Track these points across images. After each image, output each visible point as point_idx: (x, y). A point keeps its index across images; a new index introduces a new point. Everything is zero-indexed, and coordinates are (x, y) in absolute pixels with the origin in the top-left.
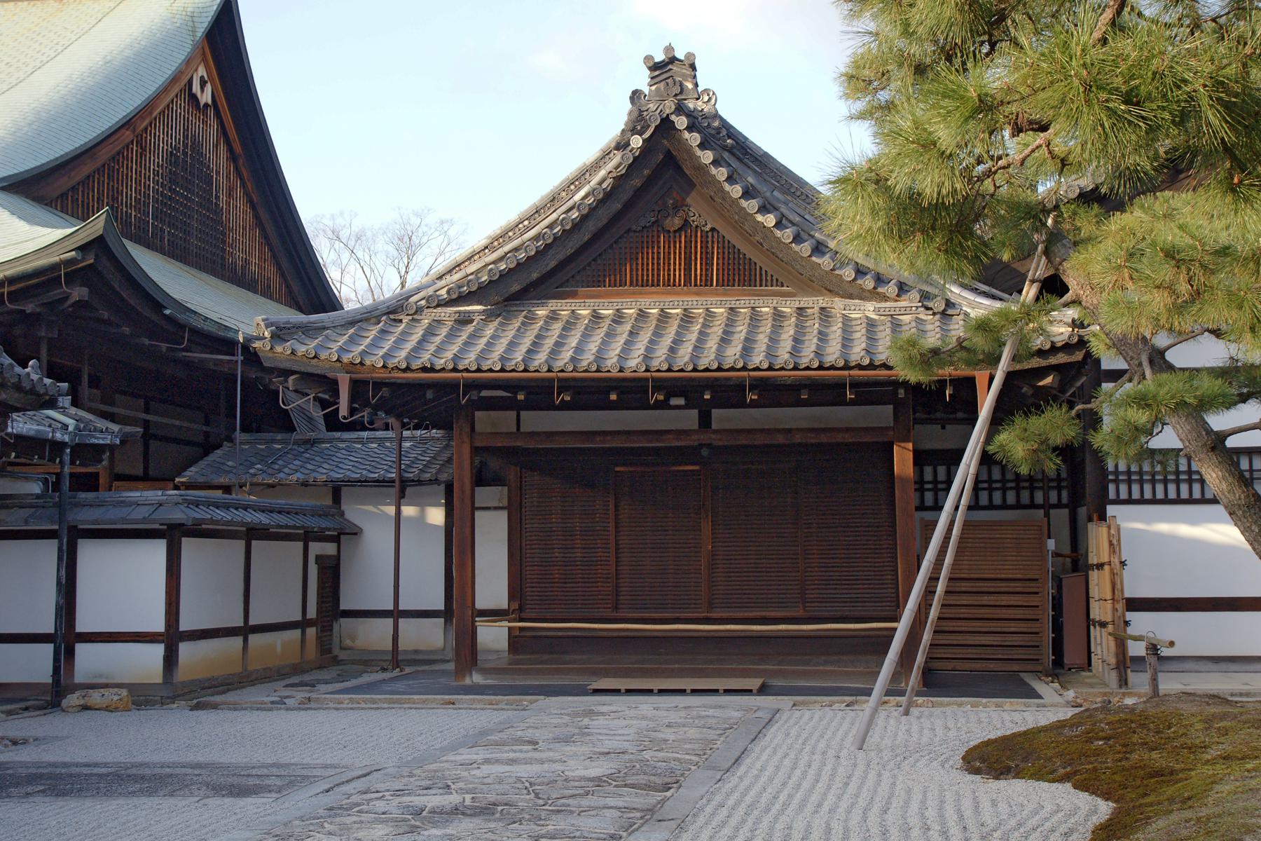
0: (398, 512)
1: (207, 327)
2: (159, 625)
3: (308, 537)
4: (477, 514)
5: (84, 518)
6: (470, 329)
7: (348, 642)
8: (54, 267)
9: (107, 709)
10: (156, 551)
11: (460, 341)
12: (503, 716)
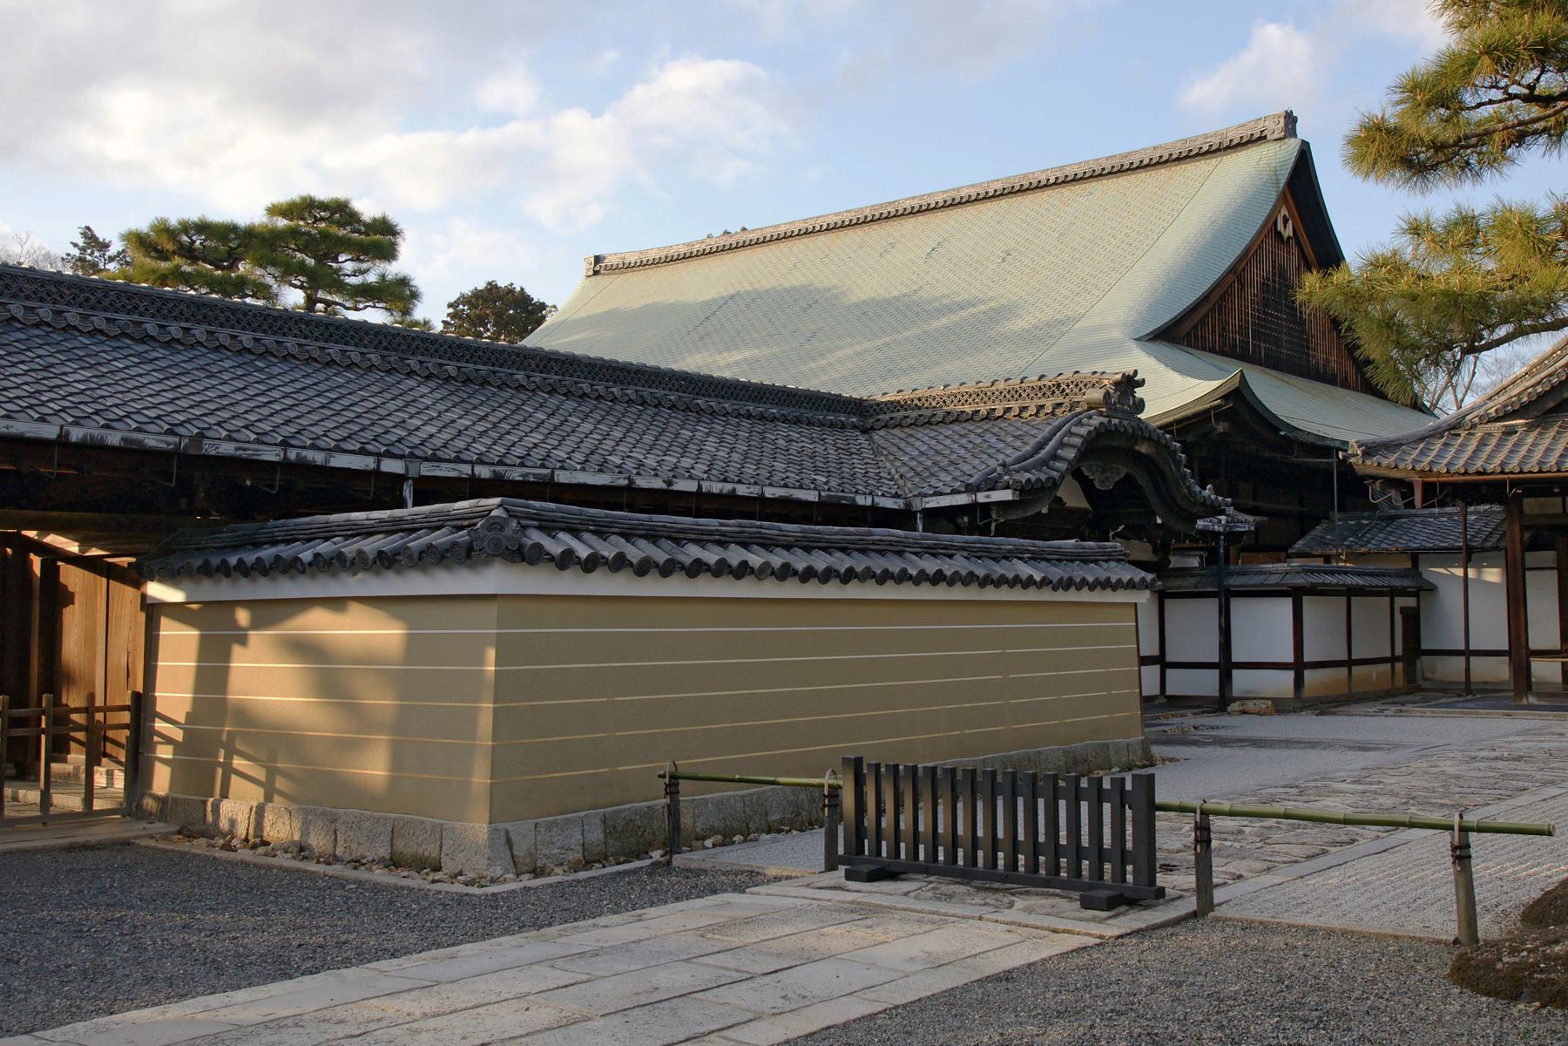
0: (1466, 573)
1: (1311, 439)
2: (1290, 659)
3: (1393, 593)
4: (1528, 573)
5: (1235, 582)
6: (1514, 438)
7: (1429, 675)
8: (1207, 411)
9: (1258, 713)
10: (1285, 606)
11: (1506, 450)
12: (1545, 723)
